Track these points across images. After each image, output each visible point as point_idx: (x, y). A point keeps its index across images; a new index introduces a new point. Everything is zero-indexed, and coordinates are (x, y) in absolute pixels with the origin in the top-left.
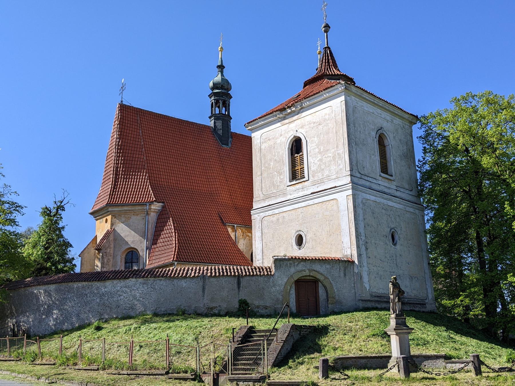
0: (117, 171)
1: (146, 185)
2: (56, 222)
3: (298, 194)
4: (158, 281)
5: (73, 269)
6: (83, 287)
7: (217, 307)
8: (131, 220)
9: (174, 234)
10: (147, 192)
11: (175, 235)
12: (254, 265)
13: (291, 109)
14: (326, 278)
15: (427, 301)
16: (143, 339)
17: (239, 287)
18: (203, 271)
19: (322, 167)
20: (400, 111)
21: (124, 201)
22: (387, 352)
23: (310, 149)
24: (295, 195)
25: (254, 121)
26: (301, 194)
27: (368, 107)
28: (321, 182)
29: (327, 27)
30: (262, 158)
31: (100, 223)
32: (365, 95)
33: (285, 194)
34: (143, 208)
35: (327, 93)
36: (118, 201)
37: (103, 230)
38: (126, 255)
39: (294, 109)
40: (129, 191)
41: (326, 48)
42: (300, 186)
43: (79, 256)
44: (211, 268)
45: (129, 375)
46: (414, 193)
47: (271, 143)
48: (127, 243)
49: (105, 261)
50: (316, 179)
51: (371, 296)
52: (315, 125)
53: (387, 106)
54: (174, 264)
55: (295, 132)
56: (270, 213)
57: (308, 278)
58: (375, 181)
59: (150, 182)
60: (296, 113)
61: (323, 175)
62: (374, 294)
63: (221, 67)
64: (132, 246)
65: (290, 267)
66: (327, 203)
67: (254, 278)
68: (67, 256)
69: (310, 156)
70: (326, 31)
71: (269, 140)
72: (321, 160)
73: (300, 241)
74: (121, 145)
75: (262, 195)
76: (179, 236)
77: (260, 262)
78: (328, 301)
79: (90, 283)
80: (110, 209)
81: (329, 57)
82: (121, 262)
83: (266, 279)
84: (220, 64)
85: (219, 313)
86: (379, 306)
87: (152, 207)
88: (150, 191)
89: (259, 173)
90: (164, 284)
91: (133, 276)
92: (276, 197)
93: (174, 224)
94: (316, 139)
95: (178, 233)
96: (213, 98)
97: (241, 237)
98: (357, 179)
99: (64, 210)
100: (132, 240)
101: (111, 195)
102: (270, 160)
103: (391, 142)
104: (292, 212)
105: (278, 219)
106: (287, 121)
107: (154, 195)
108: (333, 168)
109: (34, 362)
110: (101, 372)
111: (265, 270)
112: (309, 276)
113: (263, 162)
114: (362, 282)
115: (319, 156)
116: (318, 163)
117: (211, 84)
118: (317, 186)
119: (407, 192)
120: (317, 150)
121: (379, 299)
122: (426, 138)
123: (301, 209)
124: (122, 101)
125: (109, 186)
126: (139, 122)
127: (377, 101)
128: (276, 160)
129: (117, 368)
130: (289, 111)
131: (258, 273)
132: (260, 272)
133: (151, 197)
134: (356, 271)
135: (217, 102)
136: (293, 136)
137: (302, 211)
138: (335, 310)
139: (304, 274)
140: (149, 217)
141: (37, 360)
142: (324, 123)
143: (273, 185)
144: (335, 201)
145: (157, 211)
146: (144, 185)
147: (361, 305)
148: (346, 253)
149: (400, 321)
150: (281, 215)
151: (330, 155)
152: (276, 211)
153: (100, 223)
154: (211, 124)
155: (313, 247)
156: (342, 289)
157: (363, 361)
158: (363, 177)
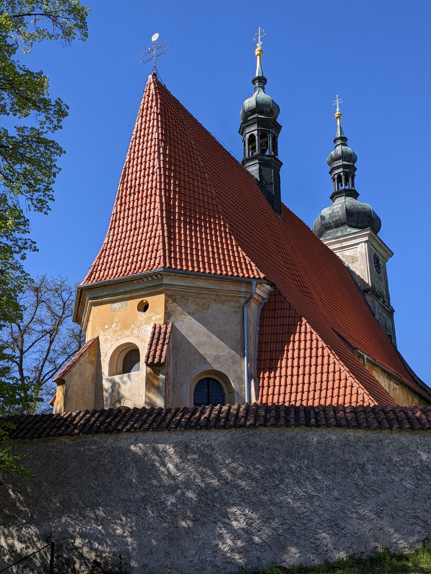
6: (346, 444)
8: (210, 311)
34: (238, 288)
48: (203, 359)
64: (216, 367)
74: (170, 156)
79: (372, 435)
80: (166, 281)
100: (214, 353)
145: (260, 300)
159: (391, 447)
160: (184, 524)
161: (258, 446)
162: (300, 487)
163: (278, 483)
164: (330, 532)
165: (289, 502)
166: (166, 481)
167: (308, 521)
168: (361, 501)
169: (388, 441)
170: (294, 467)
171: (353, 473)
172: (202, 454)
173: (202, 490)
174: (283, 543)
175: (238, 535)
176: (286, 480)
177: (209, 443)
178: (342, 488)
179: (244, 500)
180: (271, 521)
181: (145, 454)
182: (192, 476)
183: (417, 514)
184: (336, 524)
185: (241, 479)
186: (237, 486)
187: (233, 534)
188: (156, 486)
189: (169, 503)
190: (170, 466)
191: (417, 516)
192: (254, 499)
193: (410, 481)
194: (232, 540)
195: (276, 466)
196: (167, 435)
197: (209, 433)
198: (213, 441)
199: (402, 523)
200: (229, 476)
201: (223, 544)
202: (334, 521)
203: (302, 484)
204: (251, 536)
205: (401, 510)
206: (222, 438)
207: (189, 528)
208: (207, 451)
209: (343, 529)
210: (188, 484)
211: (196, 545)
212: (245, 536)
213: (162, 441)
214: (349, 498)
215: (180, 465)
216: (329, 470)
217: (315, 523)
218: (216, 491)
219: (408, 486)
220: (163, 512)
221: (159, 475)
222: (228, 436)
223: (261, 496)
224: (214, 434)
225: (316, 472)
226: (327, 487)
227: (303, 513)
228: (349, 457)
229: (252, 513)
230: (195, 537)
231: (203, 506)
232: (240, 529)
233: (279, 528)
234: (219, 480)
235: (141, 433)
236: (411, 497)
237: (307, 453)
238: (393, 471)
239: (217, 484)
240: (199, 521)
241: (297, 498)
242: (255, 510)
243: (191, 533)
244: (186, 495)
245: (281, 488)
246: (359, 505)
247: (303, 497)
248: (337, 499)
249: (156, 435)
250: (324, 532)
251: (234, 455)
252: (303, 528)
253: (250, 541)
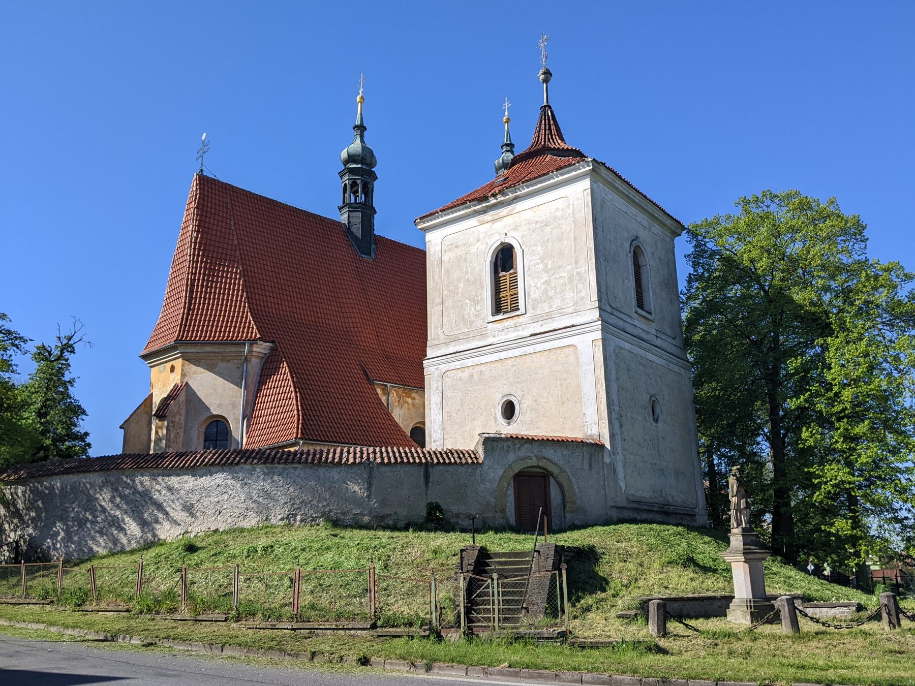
0: (192, 286)
1: (243, 312)
2: (60, 372)
4: (291, 470)
5: (84, 451)
7: (391, 515)
9: (293, 394)
10: (245, 323)
11: (296, 397)
12: (427, 448)
14: (562, 471)
15: (697, 511)
16: (287, 567)
17: (427, 483)
18: (368, 454)
19: (550, 294)
20: (661, 214)
21: (205, 337)
22: (707, 590)
23: (525, 263)
25: (431, 214)
26: (512, 335)
27: (620, 203)
28: (549, 317)
29: (548, 73)
30: (444, 277)
31: (160, 372)
32: (618, 184)
33: (483, 336)
36: (196, 337)
37: (164, 385)
38: (207, 428)
40: (214, 321)
41: (545, 106)
42: (510, 323)
43: (121, 427)
44: (361, 449)
45: (295, 630)
46: (678, 342)
47: (460, 252)
48: (207, 409)
49: (172, 436)
50: (539, 312)
51: (628, 500)
52: (538, 225)
53: (645, 204)
54: (299, 443)
55: (504, 236)
56: (458, 364)
57: (535, 470)
58: (629, 320)
59: (249, 307)
61: (551, 306)
62: (631, 498)
63: (361, 128)
64: (215, 412)
65: (508, 451)
66: (558, 352)
67: (451, 468)
68: (77, 429)
69: (529, 275)
70: (546, 81)
71: (457, 247)
72: (547, 283)
73: (509, 410)
75: (442, 336)
76: (302, 398)
77: (438, 443)
78: (565, 507)
81: (549, 121)
82: (198, 438)
83: (469, 470)
84: (358, 122)
85: (395, 524)
86: (638, 517)
87: (255, 349)
88: (250, 323)
89: (438, 301)
90: (302, 474)
91: (246, 461)
92: (467, 339)
93: (292, 378)
94: (539, 248)
95: (300, 393)
96: (346, 177)
97: (396, 404)
98: (607, 314)
99: (73, 352)
101: (184, 325)
102: (459, 280)
103: (650, 261)
104: (497, 365)
105: (471, 376)
107: (257, 328)
108: (569, 295)
109: (83, 608)
110: (234, 625)
111: (467, 455)
112: (537, 467)
113: (445, 282)
114: (616, 479)
116: (543, 287)
117: (344, 154)
118: (540, 323)
119: (669, 340)
120: (541, 266)
121: (638, 506)
122: (700, 254)
124: (201, 171)
125: (179, 310)
126: (229, 205)
127: (632, 194)
128: (468, 280)
129: (267, 618)
131: (458, 461)
132: (461, 459)
133: (252, 333)
134: (607, 460)
135: (354, 184)
136: (499, 243)
138: (577, 522)
139: (530, 463)
140: (249, 365)
141: (87, 603)
142: (555, 221)
143: (464, 319)
146: (206, 315)
147: (615, 514)
148: (589, 432)
149: (749, 540)
150: (477, 369)
151: (565, 275)
152: (469, 362)
153: (160, 372)
154: (343, 218)
155: (532, 421)
156: (586, 490)
157: (676, 605)
158: (615, 312)
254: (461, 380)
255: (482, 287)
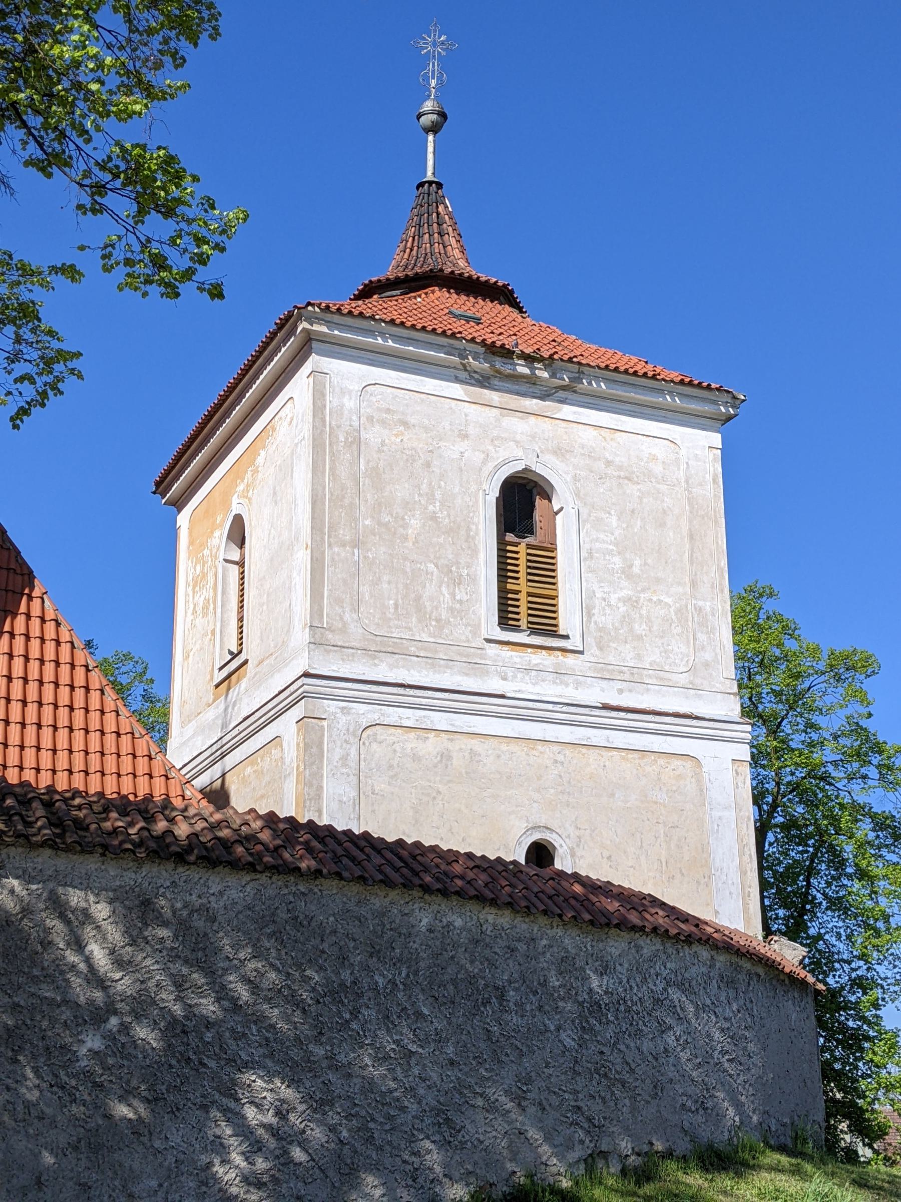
3: (537, 689)
13: (532, 369)
23: (569, 528)
24: (523, 686)
26: (550, 691)
28: (634, 678)
35: (680, 395)
39: (546, 375)
56: (409, 717)
60: (536, 390)
61: (639, 657)
66: (661, 762)
94: (614, 521)
105: (445, 756)
106: (495, 397)
115: (624, 583)
118: (619, 685)
120: (617, 562)
123: (556, 748)
130: (522, 369)
136: (520, 467)
137: (560, 758)
144: (689, 764)
151: (669, 600)
152: (440, 720)
159: (548, 955)
160: (123, 1110)
161: (314, 924)
162: (388, 1030)
163: (347, 1016)
164: (437, 1138)
165: (367, 1065)
166: (81, 991)
167: (397, 1112)
168: (492, 1070)
169: (544, 942)
170: (381, 981)
171: (485, 1007)
172: (182, 928)
173: (174, 1022)
174: (349, 1161)
175: (258, 1142)
176: (363, 1011)
177: (204, 901)
178: (464, 1037)
179: (271, 1055)
180: (327, 1108)
181: (27, 911)
182: (151, 984)
183: (579, 1103)
184: (447, 1120)
185: (269, 1000)
186: (259, 1019)
187: (246, 1136)
188: (51, 1002)
189: (83, 1050)
190: (98, 953)
191: (579, 1108)
192: (296, 1054)
193: (570, 1032)
194: (243, 1153)
195: (346, 976)
196: (93, 866)
197: (207, 876)
198: (212, 898)
199: (555, 1120)
200: (243, 993)
201: (222, 1162)
202: (444, 1113)
203: (392, 1023)
204: (284, 1143)
205: (555, 1092)
206: (234, 894)
207: (140, 1119)
208: (199, 923)
209: (459, 1131)
210: (142, 1005)
211: (161, 1165)
212: (272, 1143)
213: (77, 882)
214: (474, 1062)
215: (123, 951)
216: (444, 995)
217: (410, 1117)
218: (209, 1025)
219: (569, 1042)
220: (67, 1075)
221: (62, 973)
222: (248, 889)
223: (311, 1047)
224: (217, 880)
225: (421, 997)
226: (437, 1034)
227: (391, 1092)
228: (480, 970)
229: (288, 1086)
230: (157, 1144)
231: (174, 1062)
232: (263, 1125)
233: (340, 1125)
234: (218, 1000)
235: (20, 850)
236: (572, 1065)
237: (406, 951)
238: (547, 1007)
239: (212, 1008)
240: (162, 1103)
241: (382, 1058)
242: (293, 1082)
243: (146, 1133)
244: (132, 1033)
245: (353, 1030)
246: (488, 1079)
247: (392, 1055)
248: (452, 1063)
249: (62, 862)
250: (428, 1137)
251: (258, 940)
252: (387, 1127)
253: (283, 1159)
254: (416, 758)
255: (475, 552)
